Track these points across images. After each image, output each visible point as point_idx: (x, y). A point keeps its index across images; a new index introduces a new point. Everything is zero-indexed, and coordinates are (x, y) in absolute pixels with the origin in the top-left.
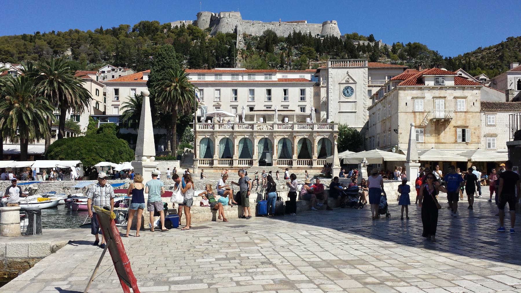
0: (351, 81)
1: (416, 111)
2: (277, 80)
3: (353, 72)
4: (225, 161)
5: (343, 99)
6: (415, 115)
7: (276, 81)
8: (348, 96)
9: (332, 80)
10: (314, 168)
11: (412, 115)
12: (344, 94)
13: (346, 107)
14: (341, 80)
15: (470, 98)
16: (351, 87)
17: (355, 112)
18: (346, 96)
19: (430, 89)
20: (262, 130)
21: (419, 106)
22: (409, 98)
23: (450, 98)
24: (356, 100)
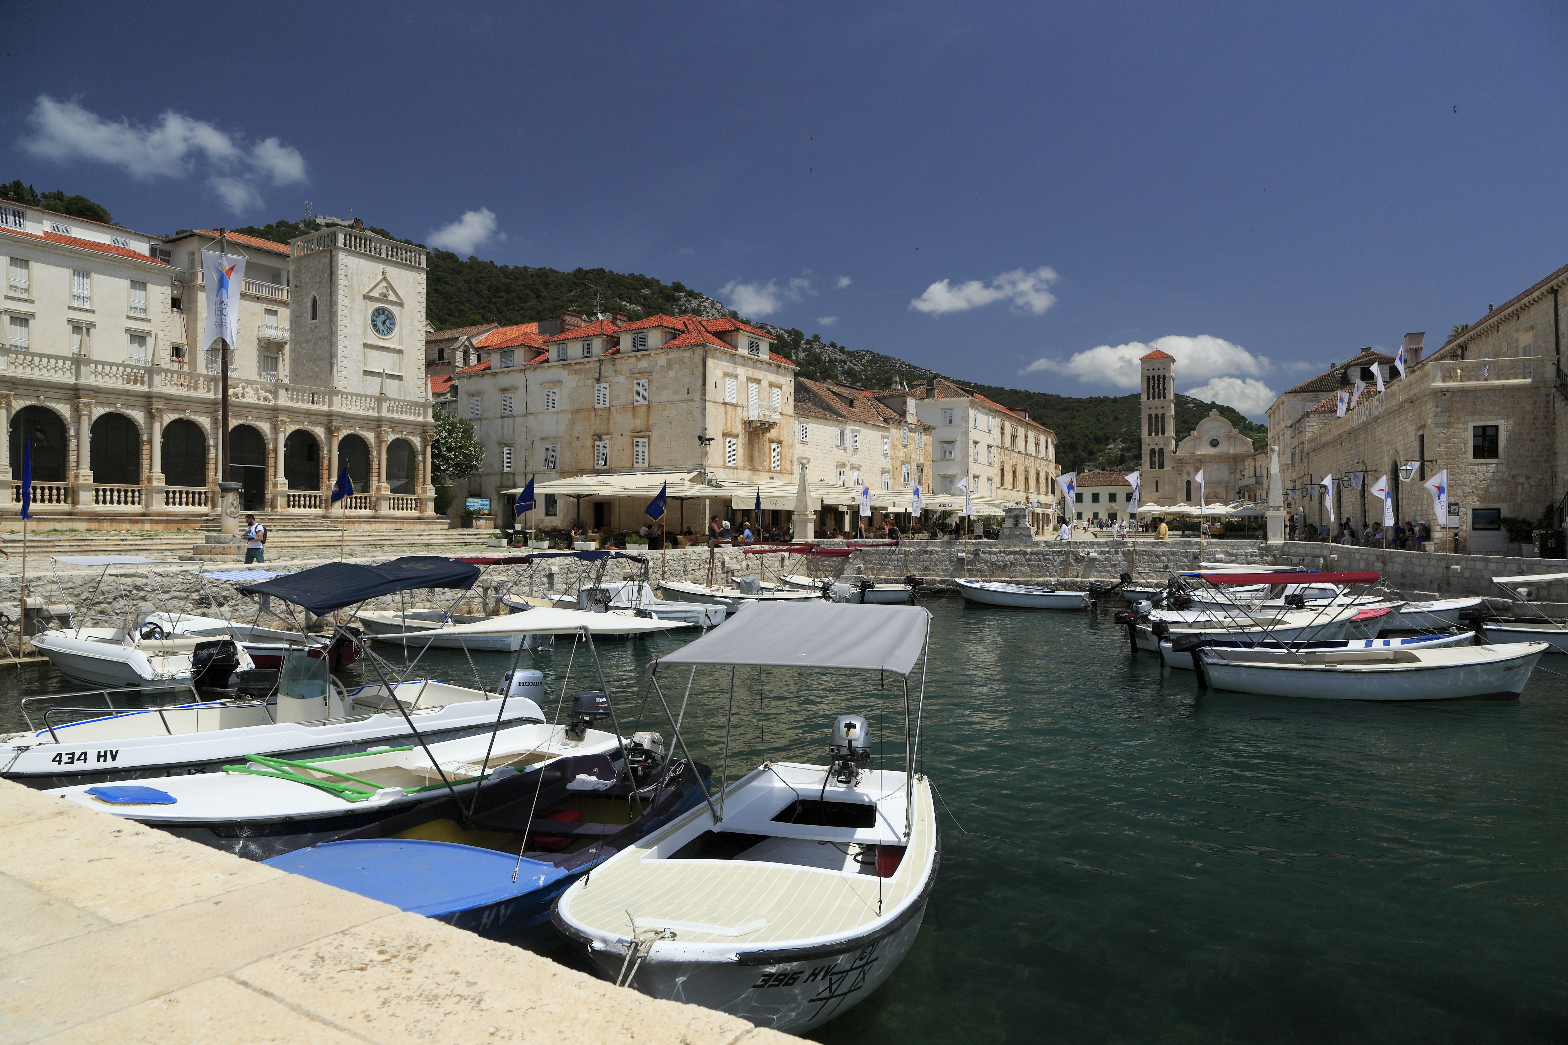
0: (392, 297)
1: (728, 401)
2: (42, 234)
3: (395, 274)
4: (112, 491)
5: (374, 339)
6: (726, 408)
7: (38, 237)
8: (383, 334)
9: (345, 283)
10: (385, 518)
11: (722, 408)
12: (375, 326)
13: (381, 362)
14: (367, 290)
15: (784, 387)
16: (390, 312)
17: (400, 378)
18: (378, 331)
19: (745, 361)
20: (244, 400)
21: (730, 391)
22: (719, 373)
23: (765, 383)
24: (401, 348)
